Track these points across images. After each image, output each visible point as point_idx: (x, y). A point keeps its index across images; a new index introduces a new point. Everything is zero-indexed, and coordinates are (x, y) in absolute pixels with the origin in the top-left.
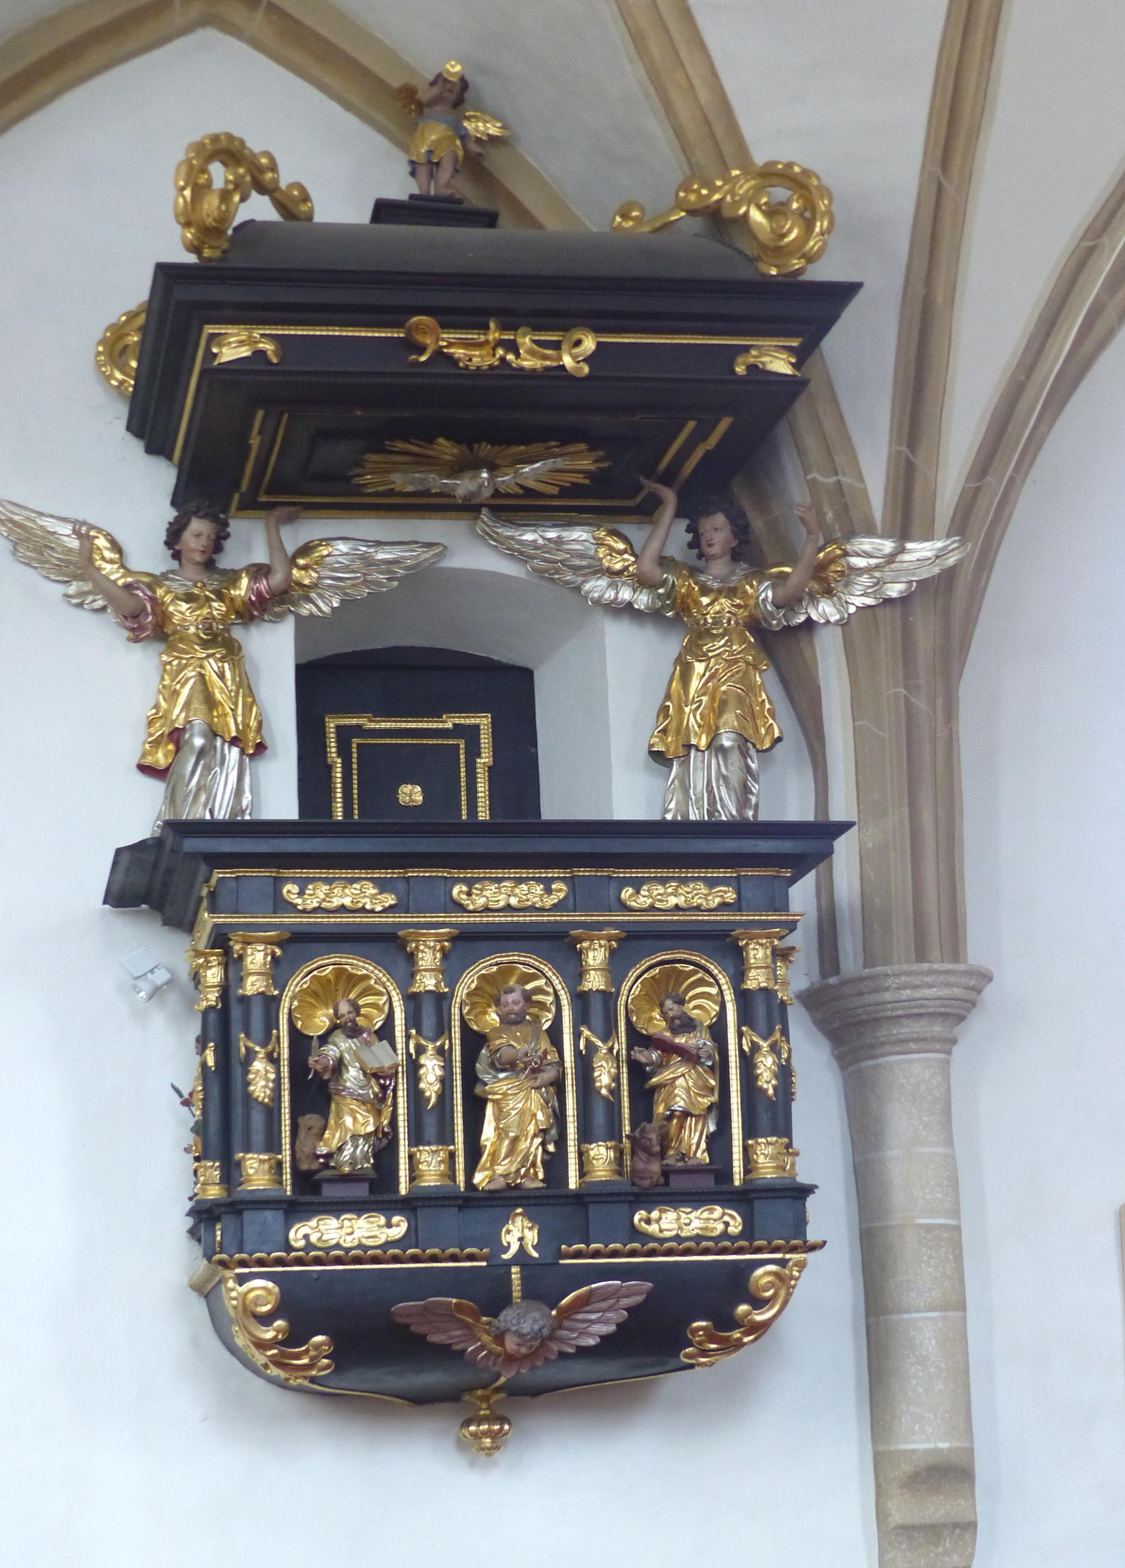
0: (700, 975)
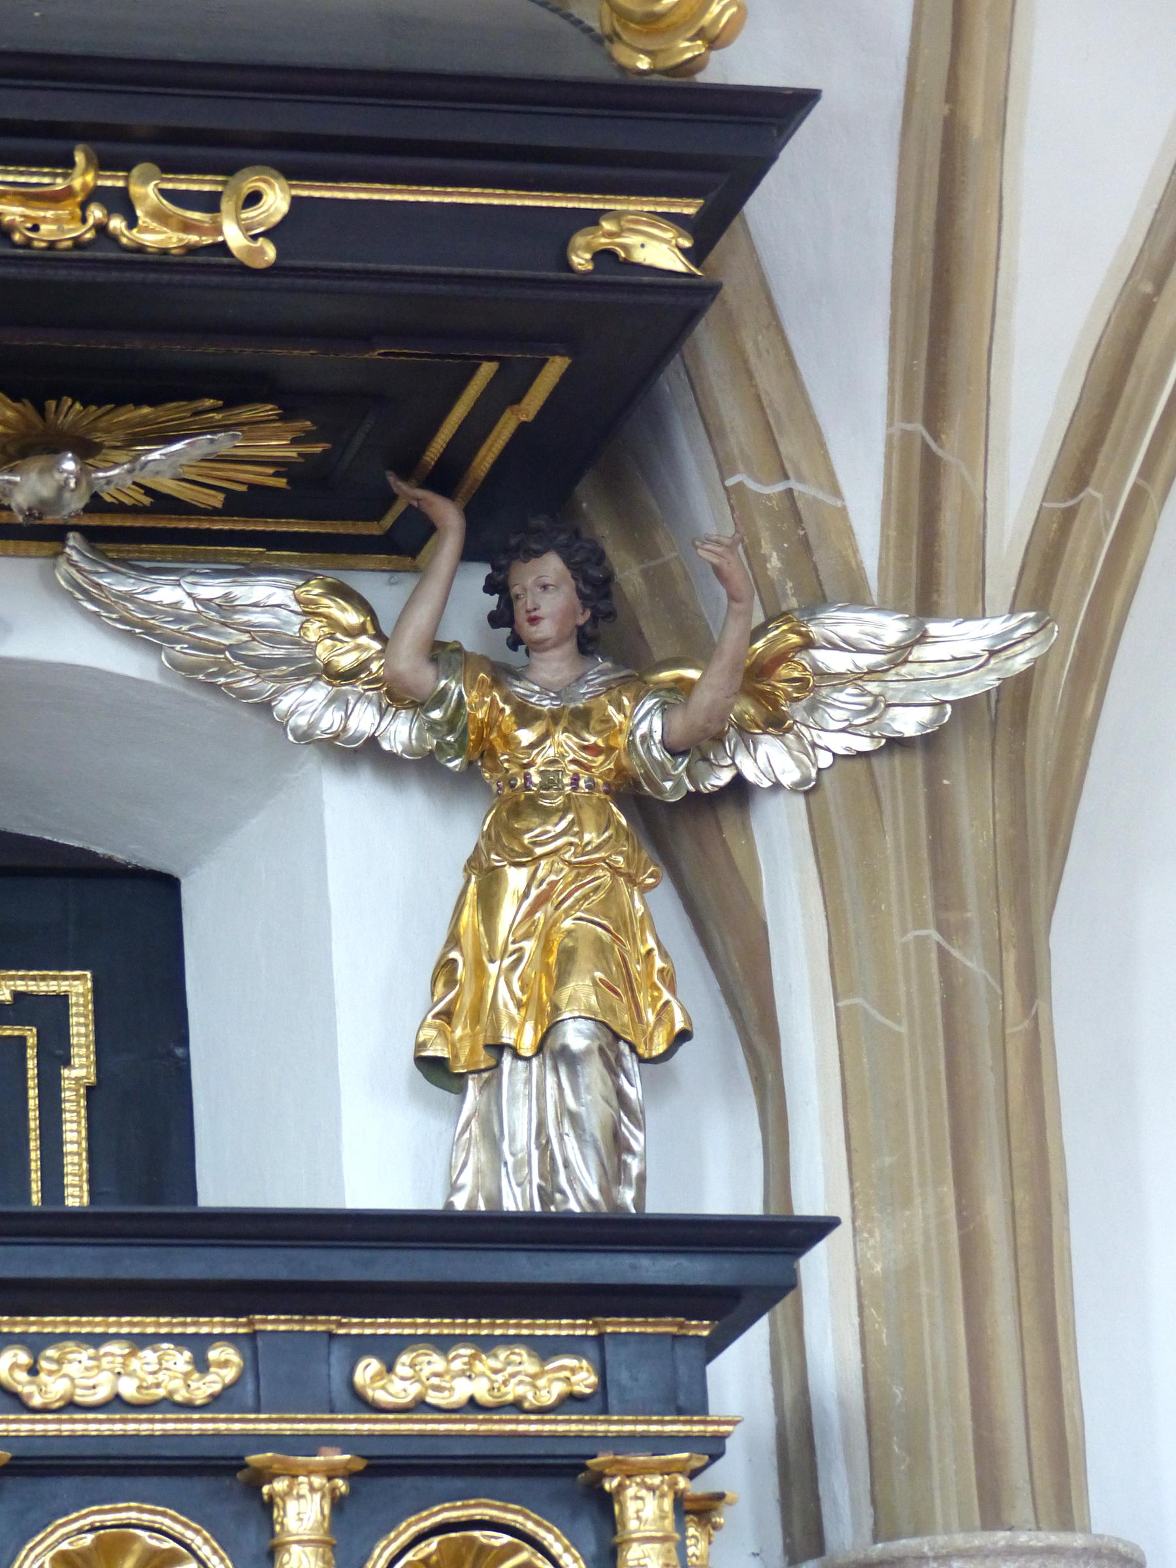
0: (523, 1557)
